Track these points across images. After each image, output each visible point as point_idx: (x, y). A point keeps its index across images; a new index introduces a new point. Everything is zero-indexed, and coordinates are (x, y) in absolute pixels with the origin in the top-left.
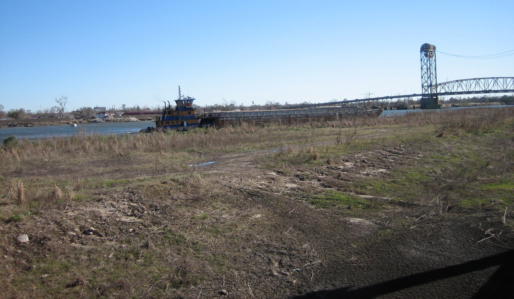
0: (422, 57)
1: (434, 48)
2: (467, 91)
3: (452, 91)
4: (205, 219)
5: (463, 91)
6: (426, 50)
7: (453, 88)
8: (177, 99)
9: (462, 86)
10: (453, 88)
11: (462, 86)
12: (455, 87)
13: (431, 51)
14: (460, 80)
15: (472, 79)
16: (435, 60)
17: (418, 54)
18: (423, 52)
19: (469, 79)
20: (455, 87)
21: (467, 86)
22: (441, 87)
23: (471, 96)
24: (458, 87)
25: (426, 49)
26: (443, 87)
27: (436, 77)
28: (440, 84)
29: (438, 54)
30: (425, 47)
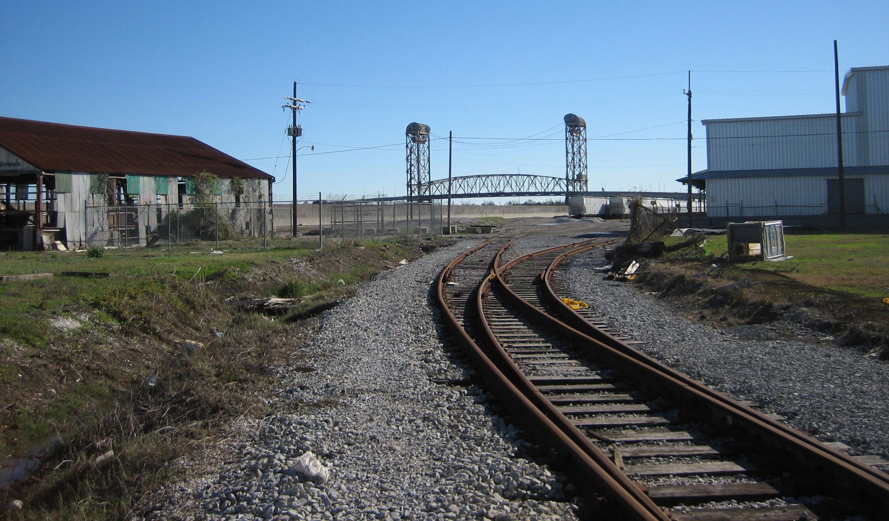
0: (408, 141)
1: (428, 129)
2: (543, 191)
3: (547, 191)
4: (6, 333)
5: (537, 191)
6: (413, 132)
7: (523, 185)
8: (684, 174)
9: (535, 185)
10: (523, 185)
11: (535, 185)
12: (526, 184)
13: (421, 134)
14: (461, 177)
15: (500, 175)
16: (429, 147)
17: (402, 138)
18: (410, 135)
19: (496, 175)
20: (526, 184)
21: (543, 184)
22: (458, 186)
23: (523, 200)
24: (529, 186)
25: (414, 130)
26: (557, 183)
27: (429, 173)
28: (455, 178)
29: (590, 132)
30: (412, 128)
